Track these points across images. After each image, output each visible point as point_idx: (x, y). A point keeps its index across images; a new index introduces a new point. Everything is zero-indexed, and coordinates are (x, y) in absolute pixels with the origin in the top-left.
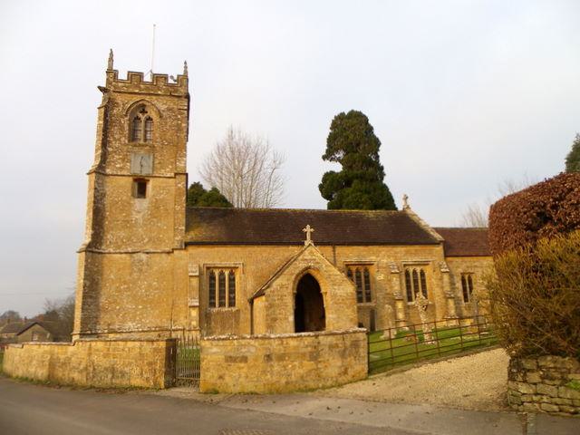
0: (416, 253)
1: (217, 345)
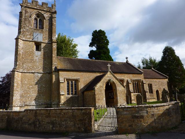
0: (136, 77)
1: (126, 111)
